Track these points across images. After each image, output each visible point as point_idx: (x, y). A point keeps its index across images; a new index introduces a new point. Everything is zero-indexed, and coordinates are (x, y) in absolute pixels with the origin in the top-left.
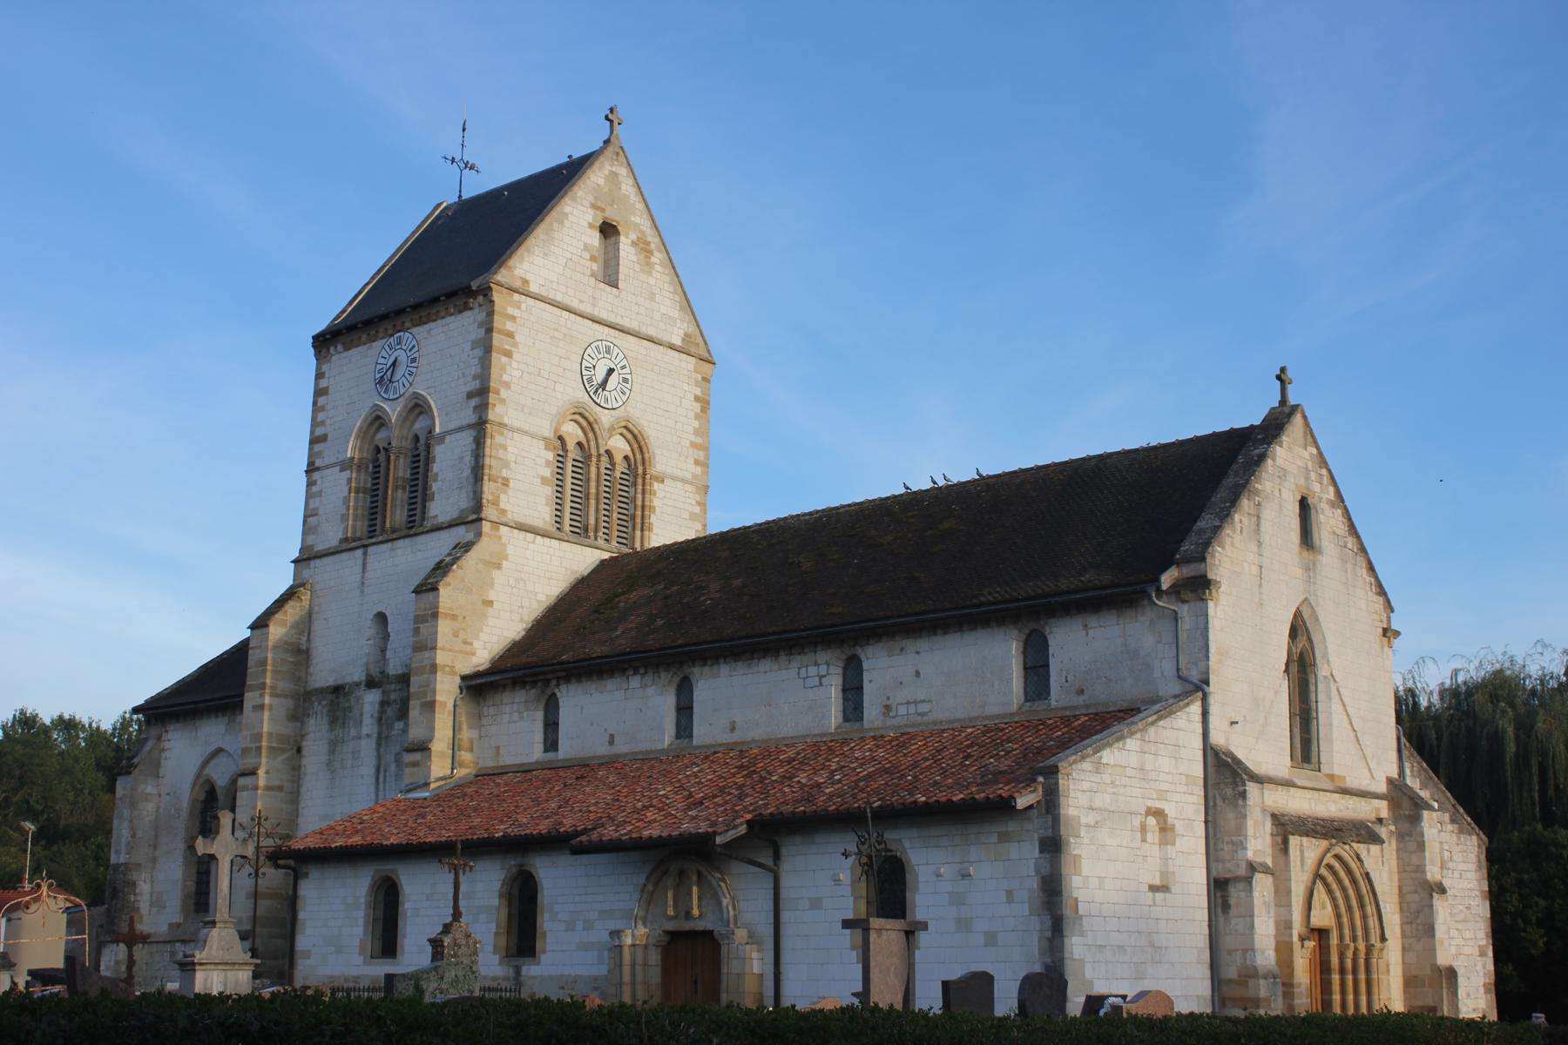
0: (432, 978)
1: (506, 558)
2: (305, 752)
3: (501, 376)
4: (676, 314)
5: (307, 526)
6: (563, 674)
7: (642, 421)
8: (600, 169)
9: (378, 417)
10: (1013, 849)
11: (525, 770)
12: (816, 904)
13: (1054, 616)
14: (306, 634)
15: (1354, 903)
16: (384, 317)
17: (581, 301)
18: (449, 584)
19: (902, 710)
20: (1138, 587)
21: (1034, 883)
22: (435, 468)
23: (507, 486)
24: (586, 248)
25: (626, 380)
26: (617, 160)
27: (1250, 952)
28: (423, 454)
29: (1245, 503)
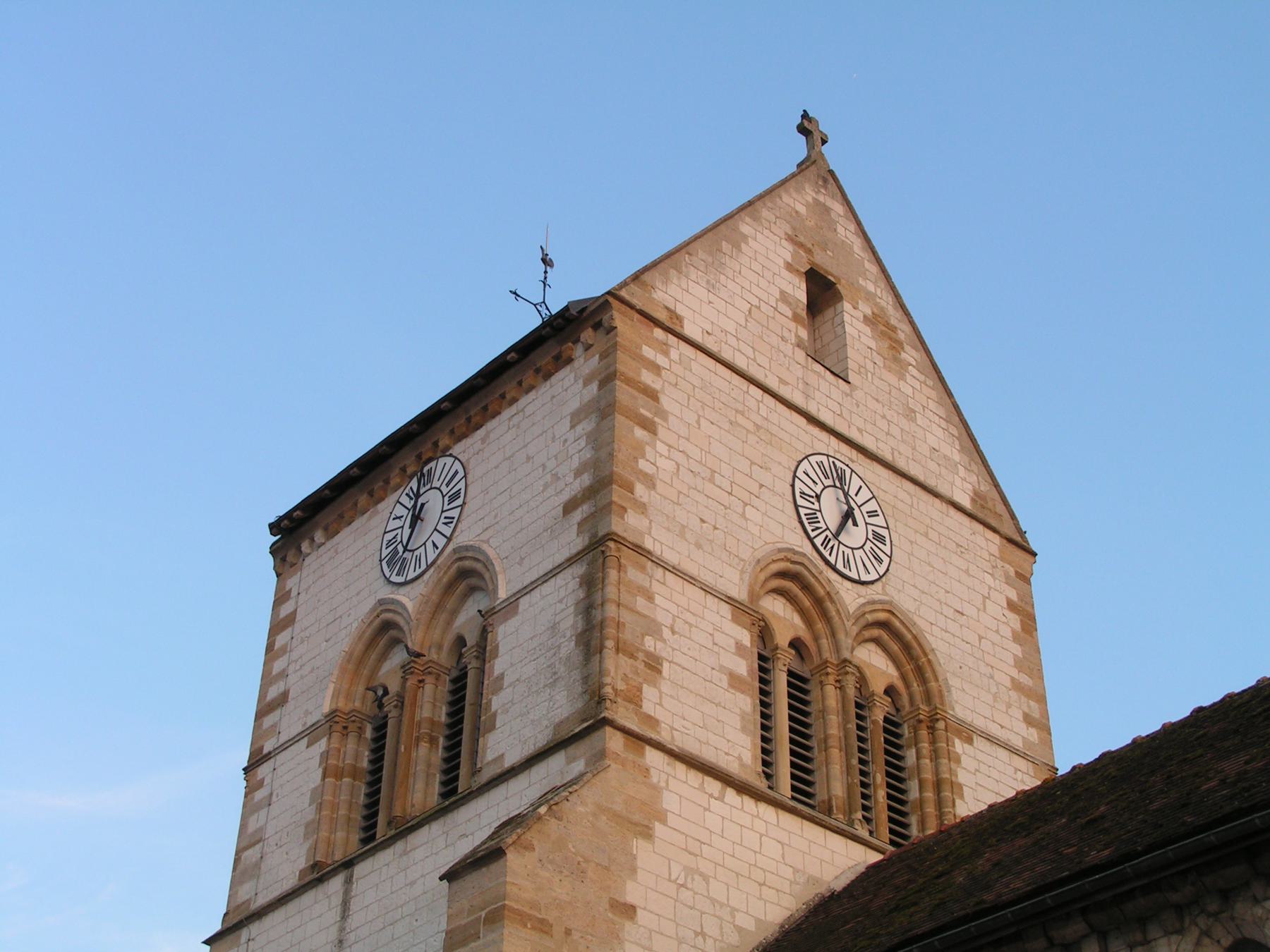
1: (662, 817)
5: (240, 867)
7: (916, 619)
9: (387, 626)
17: (782, 381)
18: (530, 847)
22: (499, 666)
23: (659, 672)
26: (826, 188)
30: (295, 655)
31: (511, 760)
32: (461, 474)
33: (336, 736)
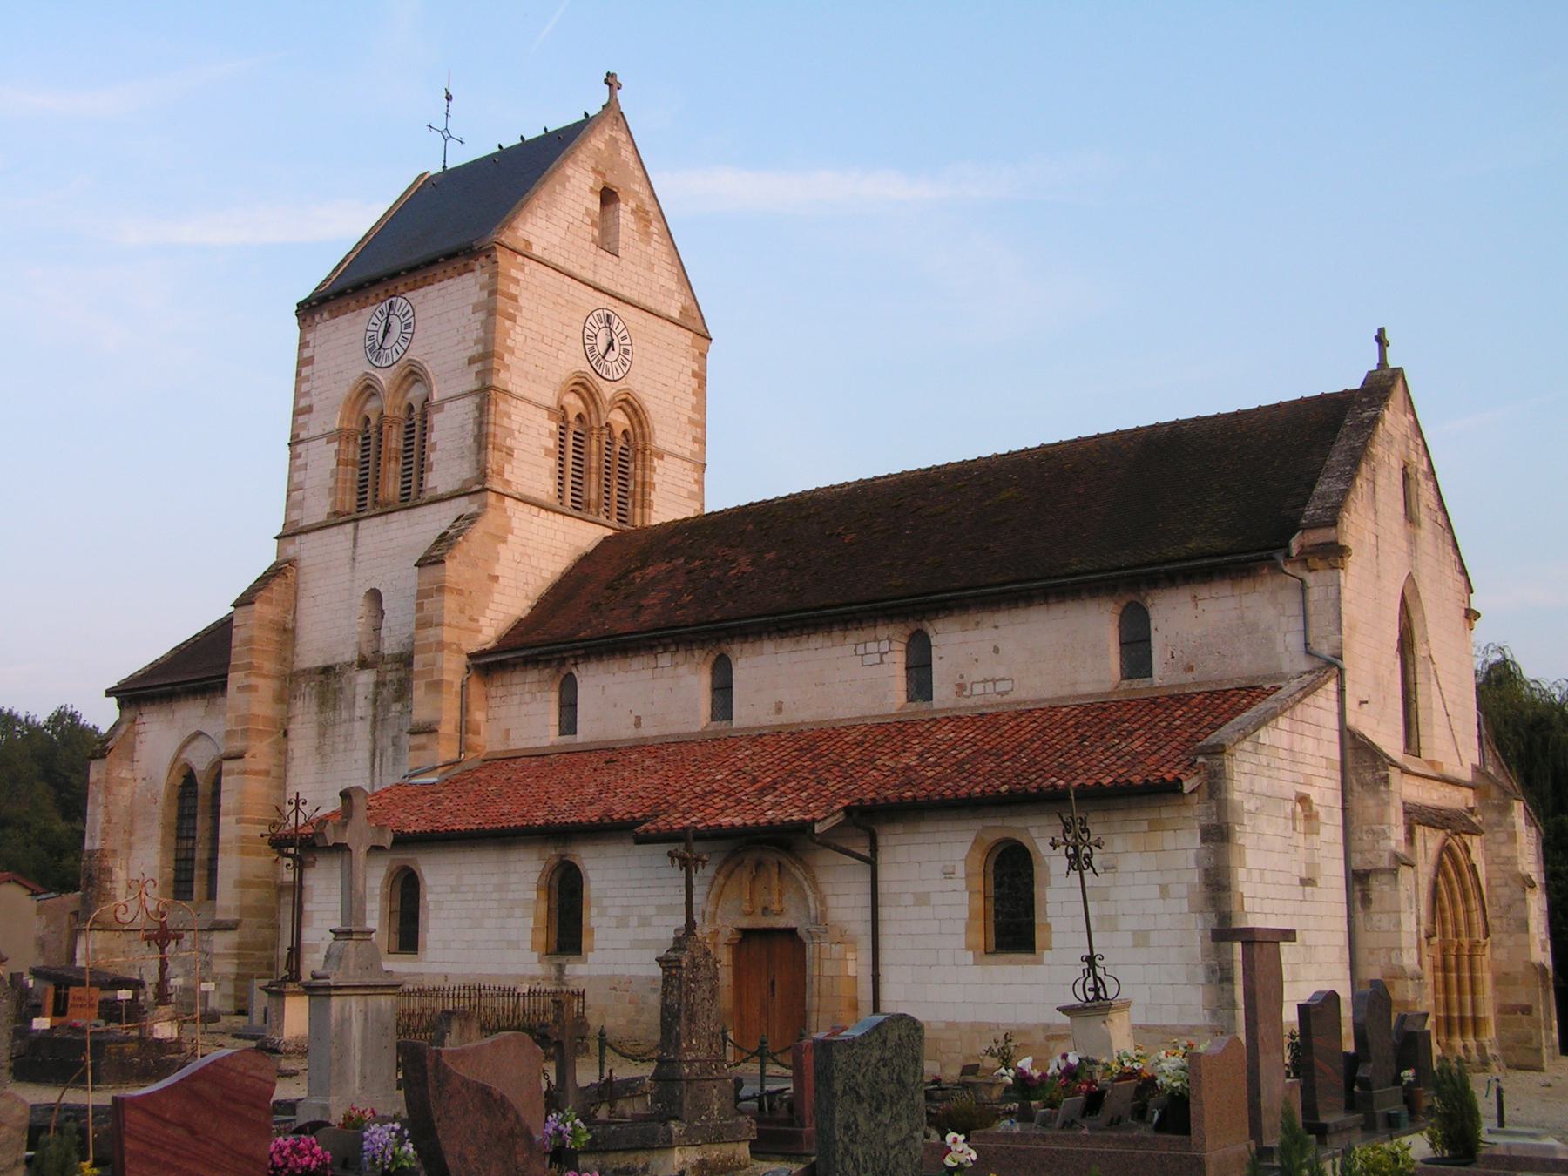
0: (875, 1043)
2: (291, 735)
3: (505, 341)
4: (673, 286)
6: (583, 652)
8: (601, 133)
9: (369, 386)
10: (1168, 839)
11: (540, 755)
12: (922, 899)
13: (1156, 587)
14: (292, 612)
15: (1458, 896)
16: (376, 282)
17: (583, 268)
18: (455, 557)
19: (978, 689)
20: (1264, 554)
21: (1195, 877)
22: (434, 437)
23: (512, 456)
24: (588, 212)
25: (626, 352)
26: (617, 125)
27: (1396, 951)
28: (418, 424)
29: (1364, 469)
30: (315, 384)
31: (441, 490)
32: (411, 313)
33: (343, 443)
